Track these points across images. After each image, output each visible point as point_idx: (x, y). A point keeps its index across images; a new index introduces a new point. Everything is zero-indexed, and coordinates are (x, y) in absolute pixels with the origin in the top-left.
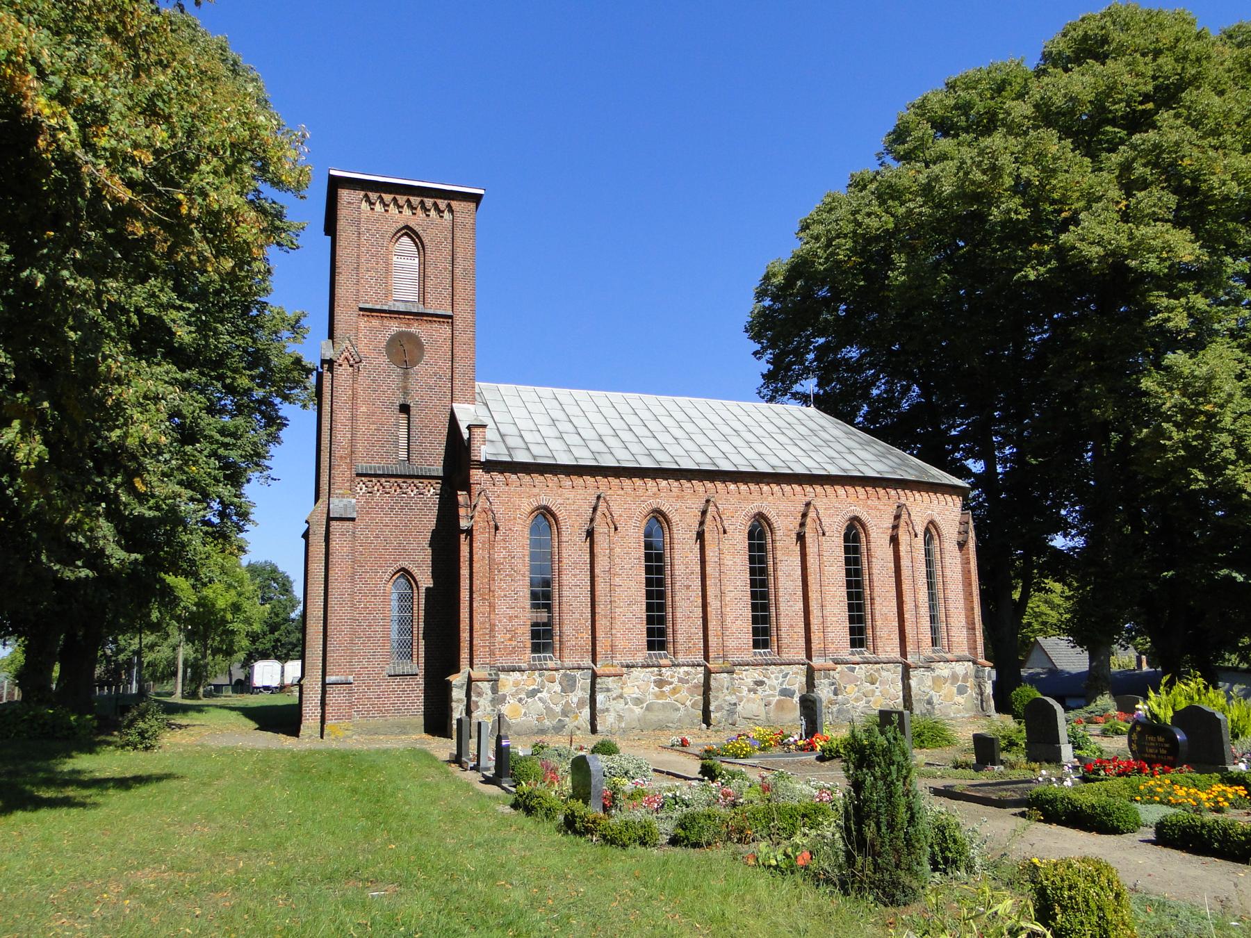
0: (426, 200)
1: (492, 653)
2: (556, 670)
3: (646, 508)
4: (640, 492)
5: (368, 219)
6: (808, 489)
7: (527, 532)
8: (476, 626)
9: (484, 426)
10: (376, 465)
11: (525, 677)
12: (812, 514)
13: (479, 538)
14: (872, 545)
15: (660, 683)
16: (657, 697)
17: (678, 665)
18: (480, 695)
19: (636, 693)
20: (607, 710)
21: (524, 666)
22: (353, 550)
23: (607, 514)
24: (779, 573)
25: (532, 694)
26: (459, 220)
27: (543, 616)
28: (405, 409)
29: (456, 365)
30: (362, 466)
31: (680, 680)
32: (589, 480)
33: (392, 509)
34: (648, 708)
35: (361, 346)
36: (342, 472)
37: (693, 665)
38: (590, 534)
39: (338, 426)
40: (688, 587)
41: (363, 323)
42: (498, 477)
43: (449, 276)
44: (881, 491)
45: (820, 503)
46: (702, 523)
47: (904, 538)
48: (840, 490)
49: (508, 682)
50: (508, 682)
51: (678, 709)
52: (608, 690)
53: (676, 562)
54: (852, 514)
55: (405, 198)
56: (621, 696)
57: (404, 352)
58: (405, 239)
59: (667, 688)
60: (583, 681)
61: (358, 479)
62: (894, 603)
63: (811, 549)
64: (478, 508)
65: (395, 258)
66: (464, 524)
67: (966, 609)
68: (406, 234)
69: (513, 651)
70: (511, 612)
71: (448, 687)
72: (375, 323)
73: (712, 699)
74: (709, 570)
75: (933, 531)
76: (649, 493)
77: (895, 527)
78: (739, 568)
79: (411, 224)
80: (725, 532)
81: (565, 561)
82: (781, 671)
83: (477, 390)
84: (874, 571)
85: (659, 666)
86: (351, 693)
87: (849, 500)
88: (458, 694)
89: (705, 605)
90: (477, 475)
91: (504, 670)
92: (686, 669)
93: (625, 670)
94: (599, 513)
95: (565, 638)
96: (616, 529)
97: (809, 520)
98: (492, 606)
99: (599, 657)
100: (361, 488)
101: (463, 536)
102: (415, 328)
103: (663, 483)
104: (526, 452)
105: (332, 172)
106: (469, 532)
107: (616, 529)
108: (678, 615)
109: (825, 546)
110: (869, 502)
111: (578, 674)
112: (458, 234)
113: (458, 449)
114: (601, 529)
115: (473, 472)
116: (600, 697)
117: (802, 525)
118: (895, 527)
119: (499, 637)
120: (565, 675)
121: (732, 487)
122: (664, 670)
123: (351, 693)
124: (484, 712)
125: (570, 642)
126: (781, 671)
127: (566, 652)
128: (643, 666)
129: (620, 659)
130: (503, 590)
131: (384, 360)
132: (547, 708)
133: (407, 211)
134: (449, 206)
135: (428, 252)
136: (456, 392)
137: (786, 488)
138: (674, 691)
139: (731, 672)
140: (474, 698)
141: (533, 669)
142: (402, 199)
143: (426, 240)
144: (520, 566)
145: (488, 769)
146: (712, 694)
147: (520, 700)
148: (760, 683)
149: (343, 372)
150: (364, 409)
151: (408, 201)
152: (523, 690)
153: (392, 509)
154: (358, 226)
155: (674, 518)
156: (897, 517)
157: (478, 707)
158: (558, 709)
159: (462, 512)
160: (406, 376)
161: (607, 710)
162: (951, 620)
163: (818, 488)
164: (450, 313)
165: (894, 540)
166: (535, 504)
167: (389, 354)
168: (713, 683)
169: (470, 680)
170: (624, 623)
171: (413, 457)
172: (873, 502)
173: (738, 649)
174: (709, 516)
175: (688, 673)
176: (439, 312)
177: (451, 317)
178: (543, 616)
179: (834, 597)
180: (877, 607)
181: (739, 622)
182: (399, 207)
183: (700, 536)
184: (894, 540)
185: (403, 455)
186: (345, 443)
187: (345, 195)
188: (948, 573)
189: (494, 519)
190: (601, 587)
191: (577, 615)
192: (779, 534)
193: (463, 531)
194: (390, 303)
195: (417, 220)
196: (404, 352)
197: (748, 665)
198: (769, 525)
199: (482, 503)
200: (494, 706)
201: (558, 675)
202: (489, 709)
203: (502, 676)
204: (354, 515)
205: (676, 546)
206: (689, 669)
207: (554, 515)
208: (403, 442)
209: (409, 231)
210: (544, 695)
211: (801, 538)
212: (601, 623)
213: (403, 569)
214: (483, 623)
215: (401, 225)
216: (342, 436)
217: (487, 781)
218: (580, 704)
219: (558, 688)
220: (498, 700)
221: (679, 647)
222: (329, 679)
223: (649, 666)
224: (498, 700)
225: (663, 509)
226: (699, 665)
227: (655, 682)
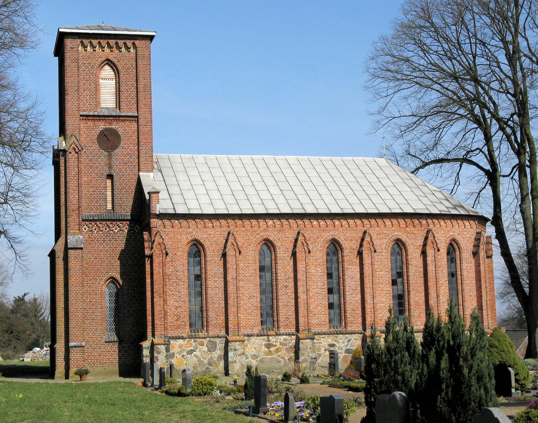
0: (119, 41)
1: (165, 329)
2: (205, 338)
4: (256, 228)
5: (83, 56)
6: (366, 222)
7: (186, 255)
8: (156, 312)
9: (158, 193)
10: (94, 213)
11: (186, 343)
12: (367, 239)
13: (157, 260)
14: (409, 257)
15: (268, 346)
16: (267, 355)
17: (280, 335)
18: (159, 353)
19: (254, 352)
20: (235, 362)
21: (185, 335)
22: (82, 266)
23: (235, 243)
24: (346, 277)
25: (191, 352)
26: (139, 53)
28: (110, 177)
29: (141, 148)
30: (86, 214)
31: (281, 344)
32: (223, 222)
33: (104, 241)
34: (261, 361)
35: (82, 139)
36: (73, 219)
37: (289, 335)
38: (224, 255)
39: (70, 191)
40: (286, 287)
41: (83, 124)
42: (167, 222)
43: (135, 90)
44: (416, 222)
46: (295, 246)
47: (430, 252)
48: (388, 222)
49: (176, 345)
50: (176, 345)
51: (279, 362)
52: (235, 350)
53: (279, 271)
54: (395, 237)
55: (106, 41)
56: (243, 354)
57: (109, 140)
58: (107, 68)
59: (272, 349)
60: (220, 344)
61: (83, 223)
62: (423, 294)
63: (367, 261)
64: (156, 243)
65: (101, 81)
66: (147, 252)
67: (477, 297)
68: (107, 64)
69: (178, 327)
70: (176, 304)
71: (140, 349)
72: (90, 123)
73: (300, 355)
74: (299, 276)
75: (455, 245)
76: (262, 229)
77: (425, 245)
78: (319, 274)
79: (111, 58)
80: (309, 252)
81: (209, 272)
82: (347, 338)
83: (155, 160)
84: (411, 274)
85: (268, 335)
86: (83, 352)
87: (393, 228)
88: (146, 352)
89: (296, 298)
90: (154, 222)
91: (173, 338)
92: (285, 337)
93: (246, 338)
94: (229, 243)
95: (210, 320)
96: (240, 252)
97: (365, 243)
98: (165, 301)
99: (230, 330)
100: (85, 228)
101: (147, 259)
102: (114, 126)
103: (270, 222)
104: (185, 206)
105: (61, 30)
106: (151, 257)
107: (240, 252)
108: (280, 304)
110: (408, 229)
111: (218, 340)
112: (139, 61)
113: (142, 205)
114: (230, 253)
115: (152, 220)
116: (231, 354)
117: (361, 246)
118: (425, 245)
119: (170, 319)
120: (210, 341)
121: (315, 223)
122: (271, 338)
123: (83, 352)
124: (161, 362)
125: (212, 322)
126: (347, 338)
127: (210, 328)
128: (258, 335)
129: (243, 331)
130: (172, 291)
131: (96, 146)
132: (199, 361)
133: (107, 50)
134: (134, 44)
135: (121, 75)
136: (141, 166)
137: (351, 222)
138: (277, 350)
139: (312, 339)
140: (155, 355)
141: (190, 337)
142: (104, 42)
143: (120, 68)
144: (182, 276)
145: (156, 385)
146: (301, 352)
147: (183, 356)
149: (72, 157)
150: (85, 179)
151: (108, 43)
152: (184, 350)
153: (104, 241)
154: (78, 63)
156: (426, 238)
157: (158, 360)
158: (206, 362)
159: (146, 244)
160: (110, 156)
161: (235, 362)
162: (466, 304)
163: (373, 221)
164: (136, 114)
165: (424, 253)
166: (190, 238)
167: (99, 143)
168: (301, 346)
169: (153, 345)
170: (246, 310)
171: (116, 207)
172: (410, 229)
173: (319, 325)
174: (299, 243)
175: (285, 340)
176: (129, 114)
177: (137, 117)
179: (382, 290)
180: (412, 296)
181: (319, 308)
182: (103, 47)
183: (294, 254)
184: (424, 253)
185: (109, 206)
186: (75, 201)
187: (69, 42)
188: (465, 273)
189: (165, 249)
190: (231, 289)
191: (217, 305)
192: (346, 252)
193: (147, 256)
194: (99, 110)
195: (113, 56)
196: (109, 140)
197: (325, 334)
199: (157, 240)
200: (167, 359)
201: (205, 341)
202: (164, 361)
203: (172, 342)
204: (82, 246)
205: (278, 261)
206: (287, 337)
207: (202, 245)
208: (109, 198)
209: (109, 62)
210: (197, 353)
211: (360, 254)
212: (232, 310)
213: (112, 278)
214: (160, 311)
215: (104, 59)
216: (73, 197)
217: (156, 389)
218: (219, 358)
219: (205, 349)
220: (169, 356)
221: (281, 324)
222: (71, 344)
223: (261, 335)
224: (169, 356)
225: (270, 238)
226: (293, 335)
227: (265, 345)
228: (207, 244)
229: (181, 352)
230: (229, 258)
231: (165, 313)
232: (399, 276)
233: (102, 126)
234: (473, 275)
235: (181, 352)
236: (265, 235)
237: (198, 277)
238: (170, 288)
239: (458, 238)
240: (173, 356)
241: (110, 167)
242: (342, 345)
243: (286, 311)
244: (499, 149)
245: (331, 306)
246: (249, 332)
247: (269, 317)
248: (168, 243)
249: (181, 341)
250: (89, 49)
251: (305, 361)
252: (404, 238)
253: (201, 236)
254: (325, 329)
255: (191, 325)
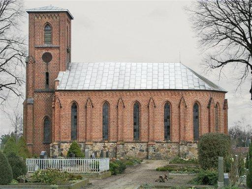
3: (102, 100)
12: (151, 101)
27: (137, 127)
45: (155, 98)
72: (39, 51)
91: (62, 142)
100: (36, 95)
109: (94, 112)
119: (62, 134)
128: (100, 142)
131: (42, 60)
139: (123, 145)
148: (134, 148)
155: (111, 103)
160: (47, 65)
178: (137, 127)
198: (199, 104)
203: (62, 144)
228: (79, 103)
229: (66, 148)
230: (150, 108)
231: (60, 132)
232: (167, 119)
233: (44, 51)
234: (177, 117)
235: (66, 148)
236: (105, 99)
237: (76, 117)
238: (63, 121)
239: (199, 100)
240: (62, 150)
241: (47, 69)
242: (138, 148)
243: (112, 132)
244: (221, 64)
245: (135, 130)
246: (96, 140)
247: (106, 135)
248: (62, 102)
249: (66, 144)
250: (39, 18)
251: (119, 154)
252: (170, 101)
253: (140, 99)
254: (132, 140)
255: (72, 137)
